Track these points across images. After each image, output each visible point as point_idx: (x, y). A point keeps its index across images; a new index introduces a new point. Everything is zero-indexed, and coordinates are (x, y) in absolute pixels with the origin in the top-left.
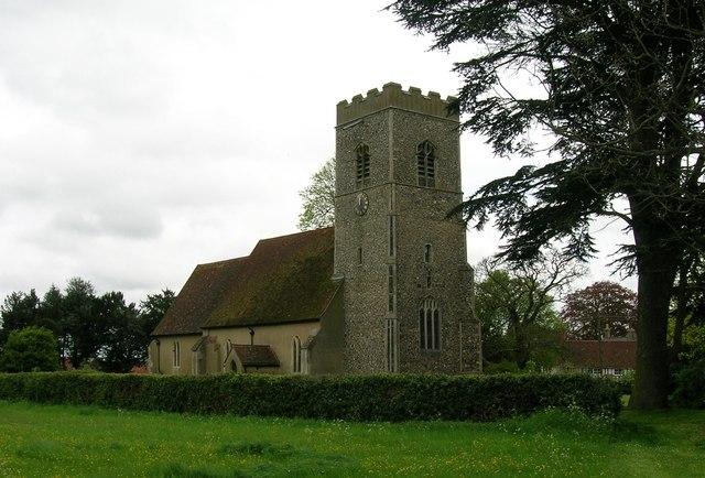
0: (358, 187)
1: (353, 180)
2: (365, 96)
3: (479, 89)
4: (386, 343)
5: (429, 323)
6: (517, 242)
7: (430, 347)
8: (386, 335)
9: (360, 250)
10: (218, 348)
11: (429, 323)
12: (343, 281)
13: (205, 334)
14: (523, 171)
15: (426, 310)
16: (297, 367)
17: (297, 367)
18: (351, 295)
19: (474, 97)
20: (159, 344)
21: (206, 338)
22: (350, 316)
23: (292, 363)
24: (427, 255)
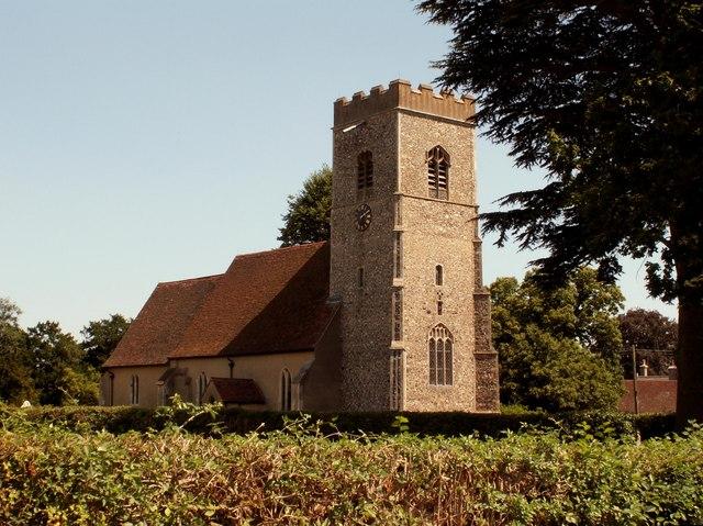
1: (354, 190)
5: (440, 355)
11: (440, 355)
18: (350, 321)
22: (349, 346)
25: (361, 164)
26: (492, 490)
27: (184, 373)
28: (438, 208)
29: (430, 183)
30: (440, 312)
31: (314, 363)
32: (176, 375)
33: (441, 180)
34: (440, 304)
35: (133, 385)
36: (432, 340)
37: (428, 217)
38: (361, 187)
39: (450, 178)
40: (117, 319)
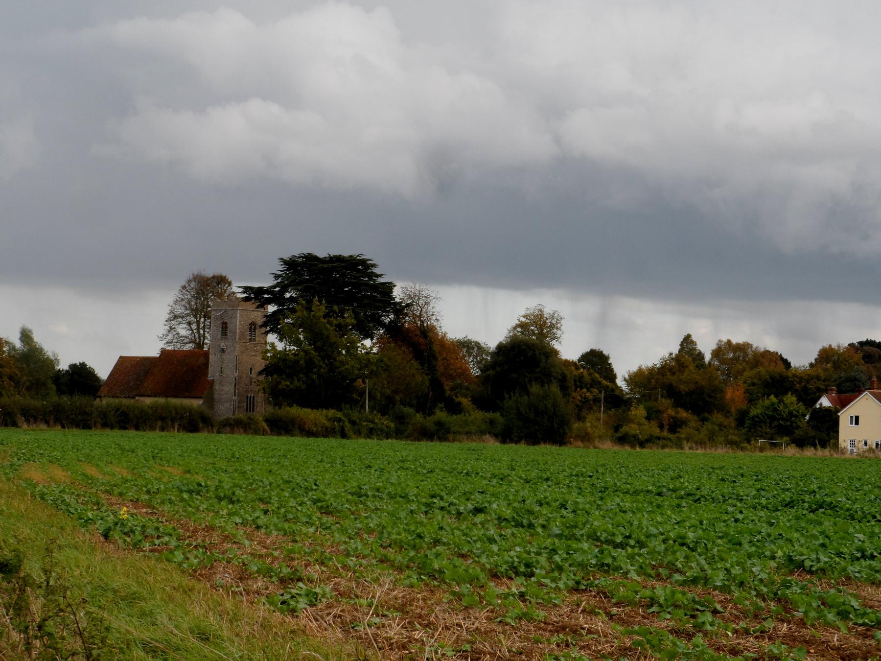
1: (219, 336)
5: (250, 400)
7: (250, 411)
11: (250, 400)
18: (217, 387)
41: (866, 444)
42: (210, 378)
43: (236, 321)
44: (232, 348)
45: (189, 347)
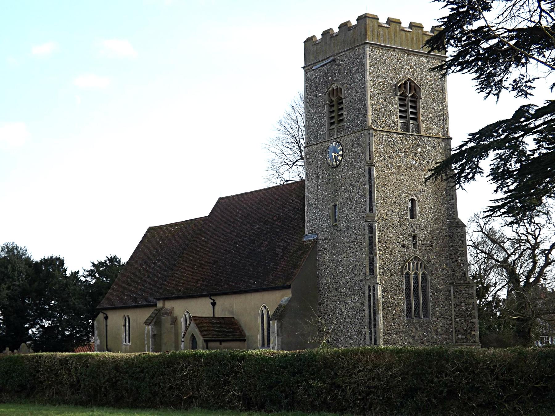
0: (330, 135)
1: (325, 128)
2: (336, 30)
3: (468, 17)
4: (367, 312)
5: (416, 289)
6: (514, 195)
7: (418, 315)
8: (367, 303)
9: (335, 206)
10: (175, 321)
11: (416, 289)
12: (316, 241)
13: (160, 304)
14: (521, 112)
15: (412, 273)
16: (266, 342)
17: (266, 342)
18: (326, 257)
19: (461, 27)
20: (106, 318)
21: (160, 310)
22: (324, 281)
23: (260, 337)
24: (412, 210)
25: (332, 101)
26: (312, 174)
27: (170, 313)
28: (409, 142)
29: (401, 117)
30: (414, 245)
31: (291, 299)
32: (163, 315)
33: (412, 113)
34: (414, 237)
35: (125, 325)
36: (407, 273)
37: (400, 150)
38: (332, 124)
39: (422, 111)
40: (113, 260)
41: (25, 247)
42: (308, 237)
43: (364, 76)
44: (358, 150)
45: (300, 180)
